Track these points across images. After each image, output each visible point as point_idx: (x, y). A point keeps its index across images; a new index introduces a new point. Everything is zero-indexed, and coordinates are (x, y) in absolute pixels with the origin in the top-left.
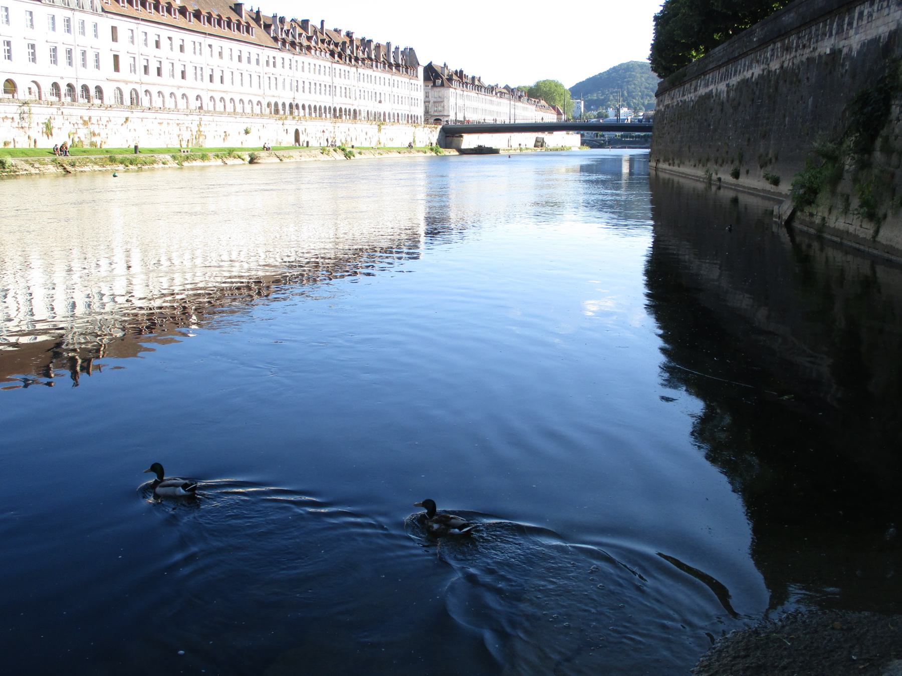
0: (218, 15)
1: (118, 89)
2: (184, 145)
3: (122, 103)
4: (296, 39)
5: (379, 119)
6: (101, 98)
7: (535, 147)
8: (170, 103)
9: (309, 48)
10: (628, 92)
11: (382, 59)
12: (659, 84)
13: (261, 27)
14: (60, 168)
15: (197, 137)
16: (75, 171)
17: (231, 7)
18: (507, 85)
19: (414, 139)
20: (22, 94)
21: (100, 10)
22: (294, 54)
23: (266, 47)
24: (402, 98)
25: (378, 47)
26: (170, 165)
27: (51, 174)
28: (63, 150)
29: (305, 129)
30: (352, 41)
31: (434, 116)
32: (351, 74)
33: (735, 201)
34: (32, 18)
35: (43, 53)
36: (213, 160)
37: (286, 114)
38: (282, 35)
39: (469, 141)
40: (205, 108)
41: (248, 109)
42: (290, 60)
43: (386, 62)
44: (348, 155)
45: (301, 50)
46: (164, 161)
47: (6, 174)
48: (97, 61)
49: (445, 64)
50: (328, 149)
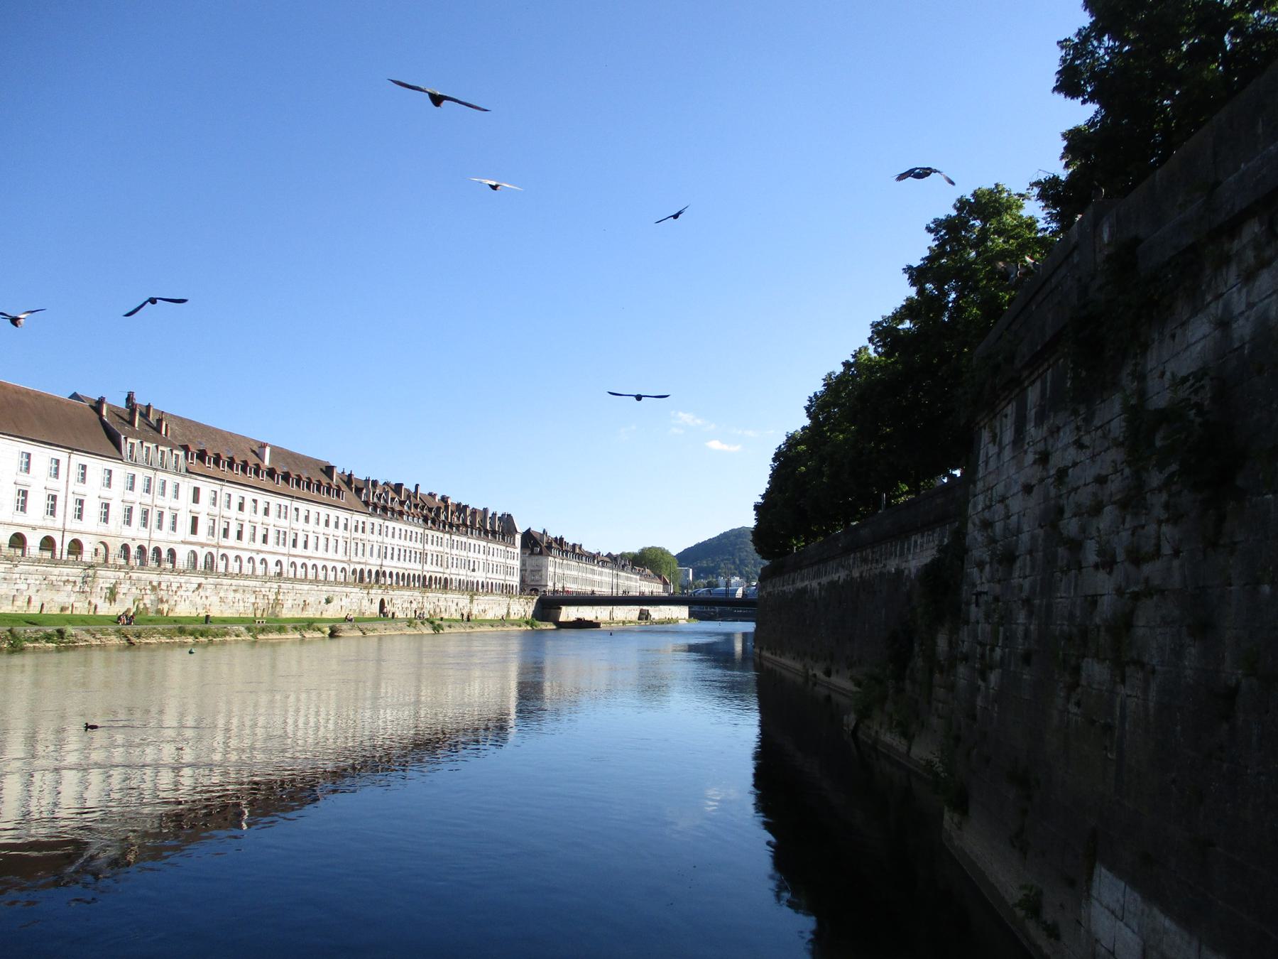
0: (308, 478)
1: (193, 552)
2: (259, 615)
3: (195, 566)
4: (388, 503)
5: (471, 589)
6: (173, 562)
7: (639, 619)
8: (247, 568)
9: (401, 513)
10: (740, 560)
11: (477, 526)
12: (1076, 142)
13: (352, 491)
14: (123, 639)
15: (274, 606)
16: (140, 642)
17: (321, 470)
18: (610, 553)
19: (508, 611)
20: (87, 556)
21: (183, 470)
22: (385, 520)
23: (356, 511)
24: (497, 566)
25: (474, 512)
26: (243, 638)
27: (113, 645)
28: (130, 619)
29: (392, 599)
30: (447, 507)
31: (532, 585)
32: (445, 541)
33: (828, 698)
34: (110, 476)
35: (117, 512)
36: (291, 632)
37: (372, 582)
38: (373, 499)
39: (569, 613)
40: (285, 575)
41: (331, 576)
42: (381, 525)
43: (482, 528)
44: (437, 628)
45: (393, 515)
46: (237, 633)
47: (63, 645)
48: (174, 523)
49: (544, 531)
50: (415, 621)
